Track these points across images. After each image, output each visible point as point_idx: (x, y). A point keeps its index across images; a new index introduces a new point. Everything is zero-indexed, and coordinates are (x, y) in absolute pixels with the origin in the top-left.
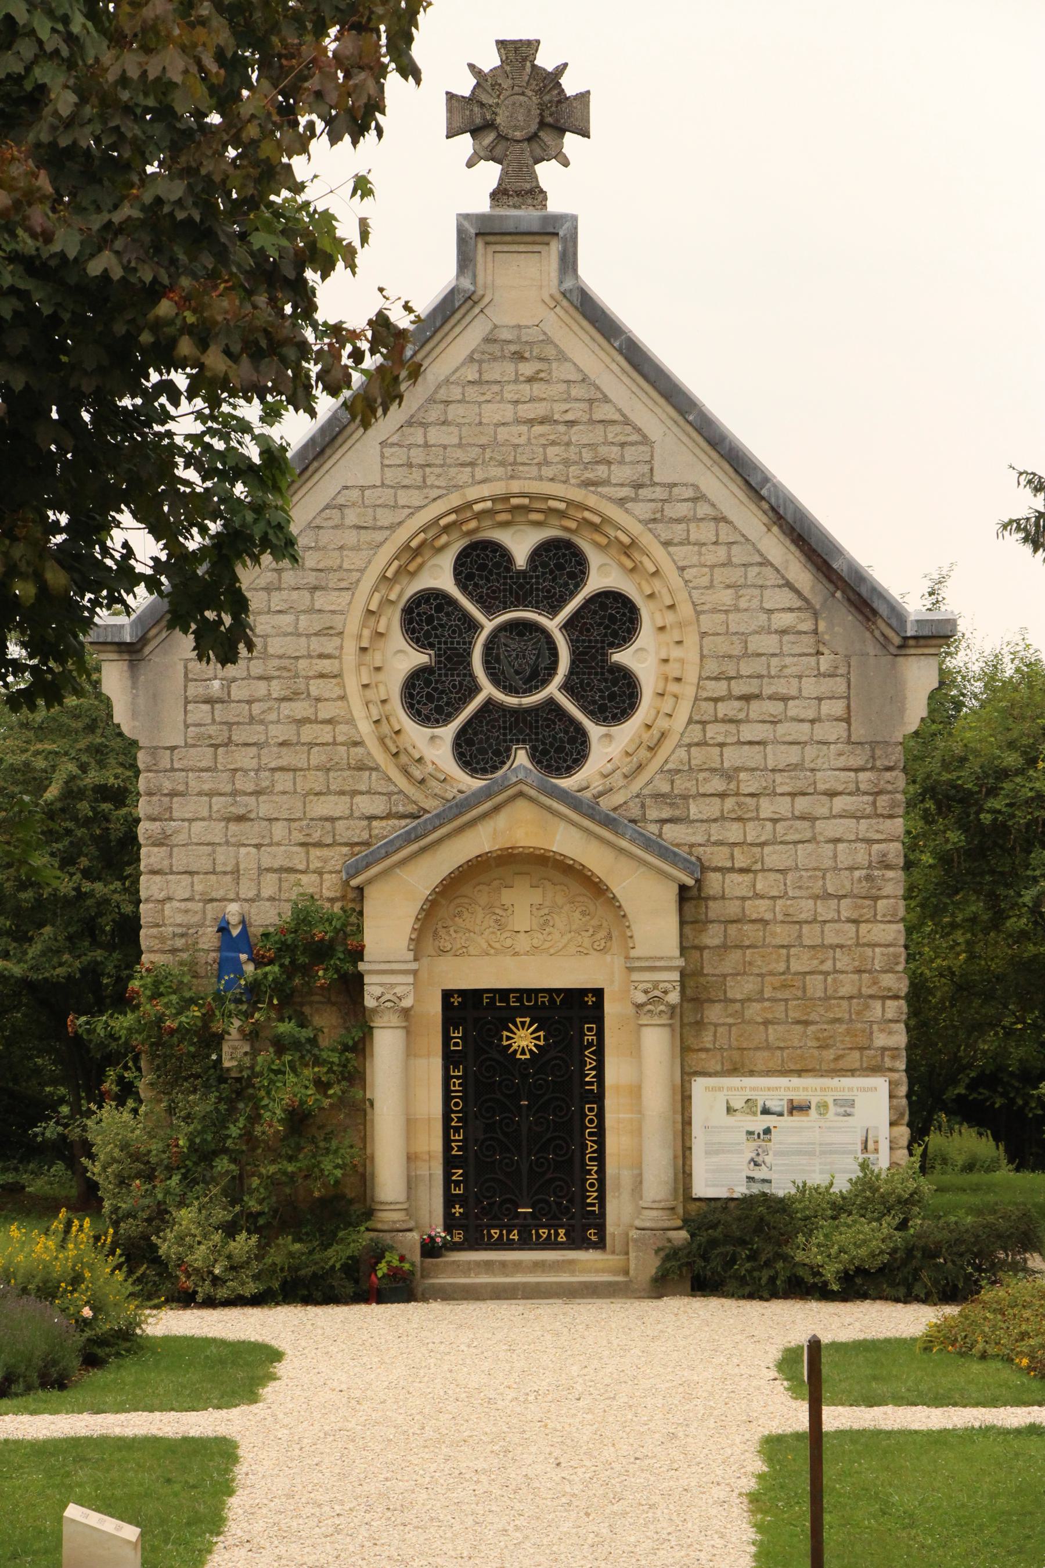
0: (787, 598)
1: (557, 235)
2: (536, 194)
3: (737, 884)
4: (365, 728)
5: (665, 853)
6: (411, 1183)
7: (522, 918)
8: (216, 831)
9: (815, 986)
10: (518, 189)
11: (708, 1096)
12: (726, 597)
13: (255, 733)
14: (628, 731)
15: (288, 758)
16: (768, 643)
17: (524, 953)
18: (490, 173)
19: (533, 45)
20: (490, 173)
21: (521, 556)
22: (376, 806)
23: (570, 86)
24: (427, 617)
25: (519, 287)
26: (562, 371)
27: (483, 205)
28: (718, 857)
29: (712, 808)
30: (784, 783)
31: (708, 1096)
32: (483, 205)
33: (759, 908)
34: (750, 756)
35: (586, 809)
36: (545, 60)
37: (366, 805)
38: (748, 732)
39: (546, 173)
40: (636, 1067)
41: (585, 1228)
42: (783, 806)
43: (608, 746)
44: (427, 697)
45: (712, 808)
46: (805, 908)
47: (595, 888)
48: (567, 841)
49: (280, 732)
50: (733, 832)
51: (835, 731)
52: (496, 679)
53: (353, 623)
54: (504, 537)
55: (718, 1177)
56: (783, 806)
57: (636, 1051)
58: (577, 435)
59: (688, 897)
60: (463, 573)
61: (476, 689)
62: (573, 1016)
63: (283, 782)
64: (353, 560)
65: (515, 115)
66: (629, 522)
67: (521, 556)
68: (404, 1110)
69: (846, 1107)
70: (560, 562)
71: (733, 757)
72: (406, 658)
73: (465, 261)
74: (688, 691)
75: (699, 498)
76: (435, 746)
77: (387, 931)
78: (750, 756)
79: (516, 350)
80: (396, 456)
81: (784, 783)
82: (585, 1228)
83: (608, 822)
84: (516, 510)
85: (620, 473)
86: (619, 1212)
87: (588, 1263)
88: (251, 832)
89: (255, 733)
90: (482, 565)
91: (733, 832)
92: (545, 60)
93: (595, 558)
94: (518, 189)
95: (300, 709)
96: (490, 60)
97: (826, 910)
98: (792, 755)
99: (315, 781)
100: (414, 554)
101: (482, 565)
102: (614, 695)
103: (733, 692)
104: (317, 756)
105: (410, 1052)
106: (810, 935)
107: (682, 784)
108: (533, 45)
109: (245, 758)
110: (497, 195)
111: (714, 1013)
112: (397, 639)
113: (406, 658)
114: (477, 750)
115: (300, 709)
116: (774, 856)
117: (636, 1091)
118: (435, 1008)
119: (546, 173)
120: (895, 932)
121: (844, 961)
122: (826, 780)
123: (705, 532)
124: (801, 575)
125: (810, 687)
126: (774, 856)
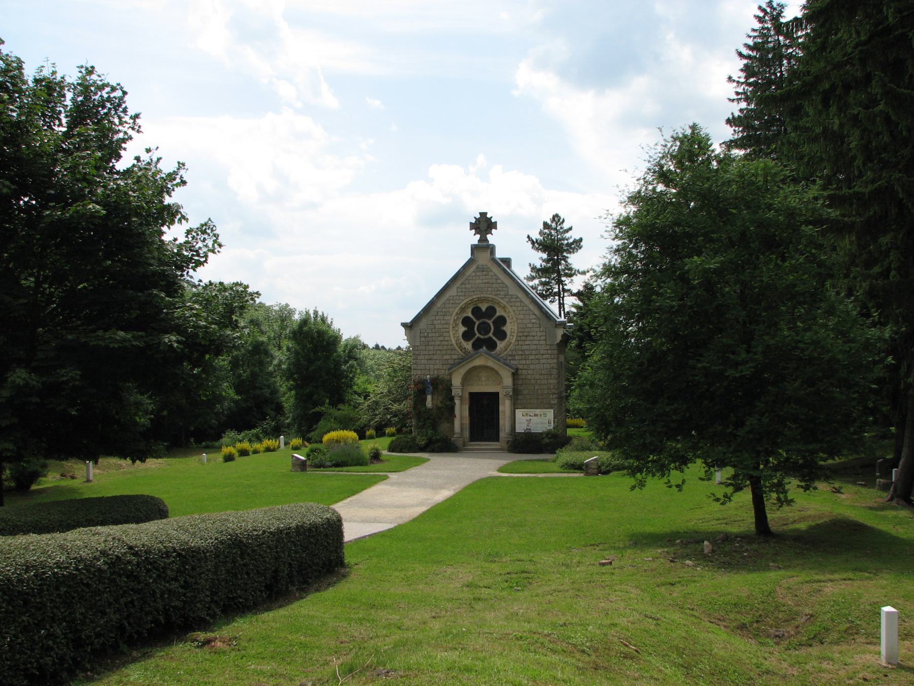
0: (533, 317)
1: (492, 249)
2: (487, 240)
3: (524, 372)
4: (454, 342)
5: (510, 367)
6: (462, 429)
7: (483, 379)
8: (426, 362)
9: (540, 392)
10: (483, 239)
11: (519, 413)
12: (522, 317)
13: (433, 343)
14: (504, 343)
15: (441, 348)
16: (530, 325)
17: (484, 386)
18: (478, 236)
19: (496, 228)
20: (478, 236)
21: (484, 309)
22: (456, 357)
23: (493, 220)
24: (466, 322)
25: (483, 258)
26: (491, 274)
27: (476, 243)
28: (520, 367)
29: (520, 357)
30: (534, 352)
31: (519, 413)
32: (476, 243)
33: (529, 377)
34: (527, 347)
35: (497, 358)
36: (489, 216)
37: (454, 357)
38: (527, 343)
39: (489, 236)
40: (505, 407)
41: (497, 439)
42: (533, 357)
43: (501, 345)
44: (467, 336)
45: (520, 357)
46: (538, 377)
47: (497, 373)
48: (490, 363)
49: (437, 343)
50: (524, 362)
51: (544, 342)
52: (489, 325)
53: (452, 322)
54: (480, 305)
55: (520, 428)
56: (533, 357)
57: (504, 404)
58: (494, 286)
59: (515, 375)
60: (473, 312)
61: (493, 323)
62: (494, 397)
63: (438, 352)
64: (451, 310)
65: (483, 226)
66: (504, 302)
67: (484, 309)
68: (462, 412)
69: (545, 415)
70: (491, 310)
71: (524, 347)
72: (462, 329)
73: (472, 253)
74: (515, 335)
75: (517, 297)
76: (468, 346)
77: (456, 381)
78: (527, 347)
79: (483, 269)
80: (459, 290)
81: (534, 352)
82: (497, 439)
83: (499, 361)
84: (481, 300)
85: (502, 293)
86: (502, 435)
87: (494, 445)
88: (432, 362)
89: (433, 343)
90: (476, 311)
91: (524, 362)
92: (489, 216)
93: (498, 309)
94: (483, 239)
95: (441, 338)
96: (478, 216)
97: (542, 377)
98: (535, 347)
99: (444, 352)
100: (463, 309)
101: (476, 311)
102: (502, 335)
103: (523, 335)
104: (445, 347)
105: (461, 404)
106: (539, 382)
107: (514, 353)
108: (496, 228)
109: (431, 348)
110: (479, 241)
111: (520, 397)
112: (461, 325)
113: (462, 329)
114: (477, 346)
115: (441, 338)
116: (532, 367)
117: (504, 412)
118: (467, 396)
119: (489, 236)
120: (555, 381)
121: (545, 387)
122: (542, 352)
123: (519, 304)
124: (537, 312)
125: (539, 334)
126: (532, 367)
